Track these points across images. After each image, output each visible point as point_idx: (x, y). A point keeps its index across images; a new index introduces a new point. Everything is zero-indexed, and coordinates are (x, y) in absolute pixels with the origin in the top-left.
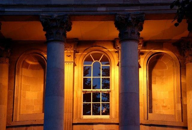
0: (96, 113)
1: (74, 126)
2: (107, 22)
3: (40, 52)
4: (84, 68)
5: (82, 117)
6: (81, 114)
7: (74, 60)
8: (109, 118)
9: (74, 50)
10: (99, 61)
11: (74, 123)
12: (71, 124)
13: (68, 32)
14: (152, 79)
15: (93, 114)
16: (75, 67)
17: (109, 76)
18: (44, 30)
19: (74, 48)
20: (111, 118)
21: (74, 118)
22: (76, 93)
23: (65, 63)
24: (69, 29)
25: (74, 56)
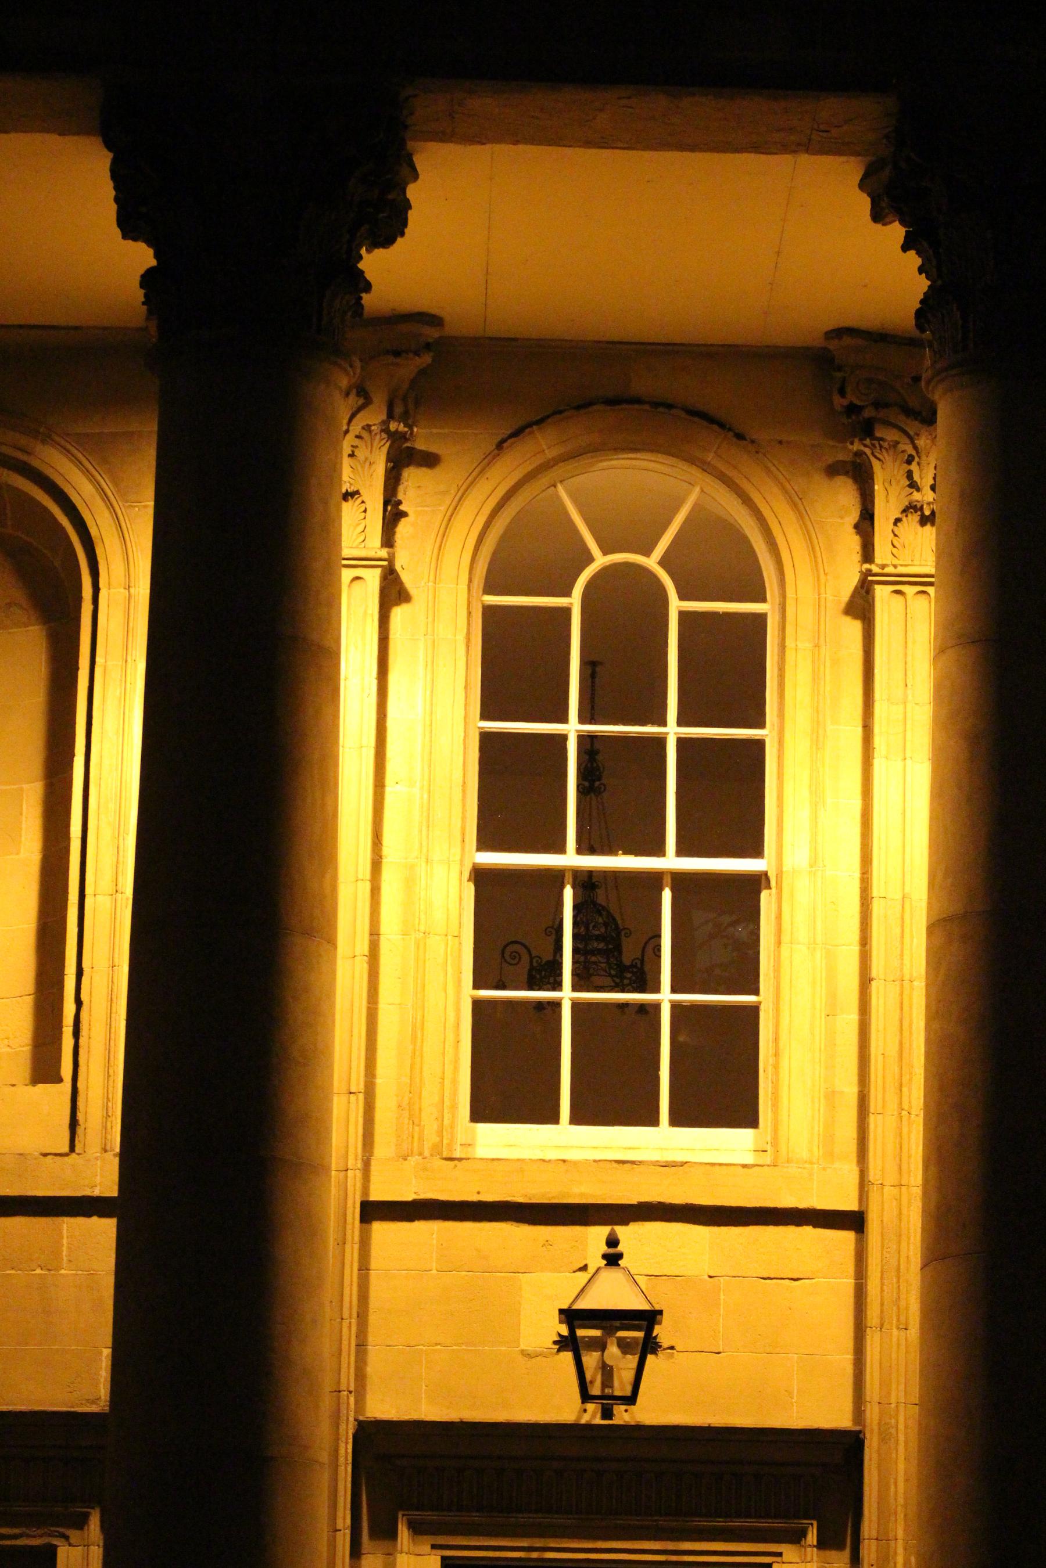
0: (614, 1096)
1: (380, 1229)
2: (780, 164)
3: (23, 441)
4: (494, 621)
5: (460, 1138)
6: (454, 1107)
7: (388, 541)
8: (749, 1159)
9: (396, 438)
10: (647, 553)
11: (375, 1196)
12: (354, 1213)
13: (368, 251)
14: (15, 485)
15: (685, 1116)
16: (398, 614)
17: (761, 725)
18: (130, 225)
19: (390, 416)
20: (774, 1156)
21: (382, 1150)
22: (409, 883)
23: (347, 575)
24: (388, 223)
25: (386, 503)
